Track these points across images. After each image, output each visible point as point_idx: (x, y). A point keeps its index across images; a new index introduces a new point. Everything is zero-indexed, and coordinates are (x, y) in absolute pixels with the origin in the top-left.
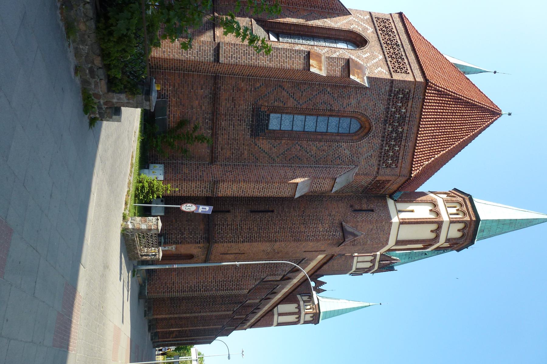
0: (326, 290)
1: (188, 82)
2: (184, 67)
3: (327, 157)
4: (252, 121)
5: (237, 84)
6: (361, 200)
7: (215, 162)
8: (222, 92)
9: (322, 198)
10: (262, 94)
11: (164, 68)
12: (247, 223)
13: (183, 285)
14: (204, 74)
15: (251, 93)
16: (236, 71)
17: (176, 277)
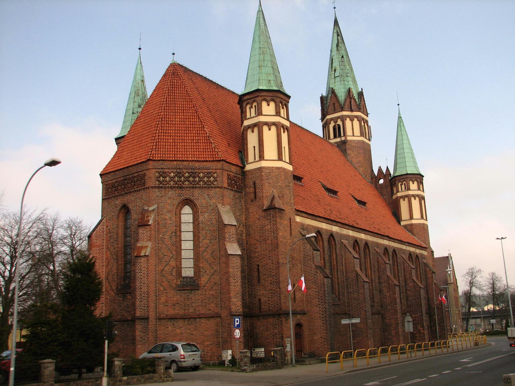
0: (387, 167)
2: (154, 341)
3: (211, 231)
4: (188, 290)
7: (219, 314)
8: (169, 313)
12: (267, 285)
13: (322, 330)
15: (168, 293)
16: (154, 305)
17: (317, 336)
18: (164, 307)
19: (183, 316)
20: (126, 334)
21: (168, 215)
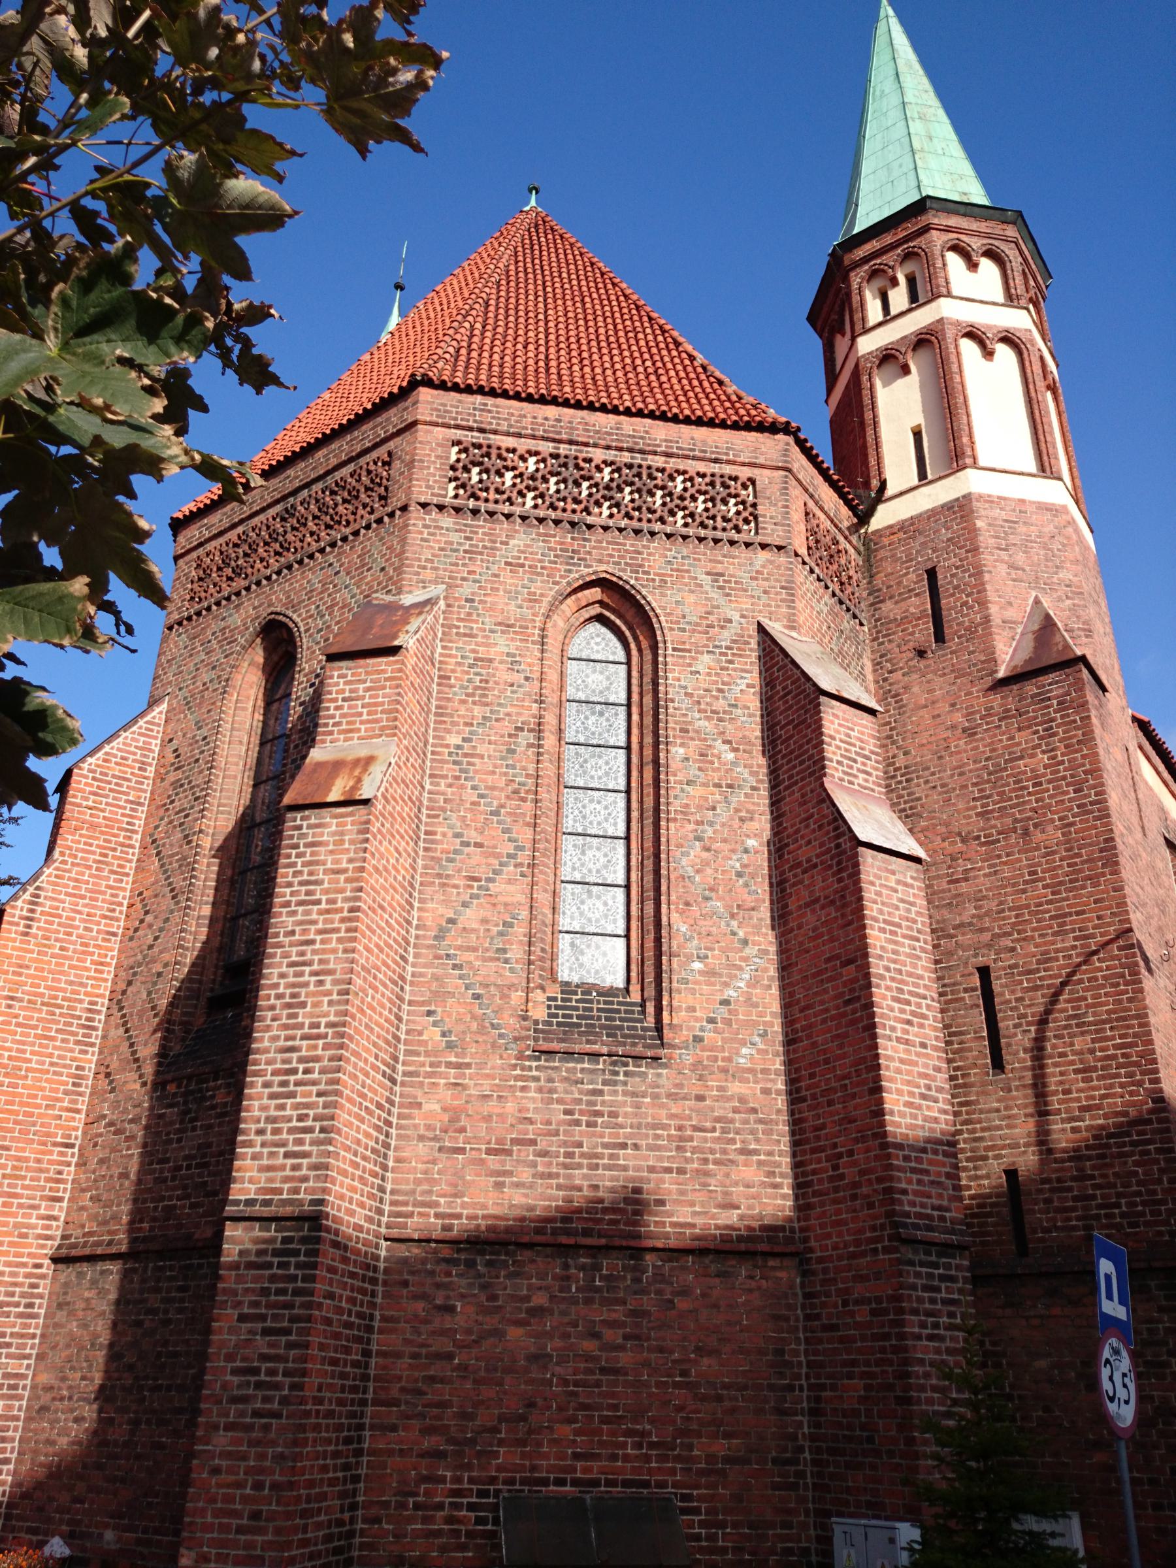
1: (416, 1381)
2: (341, 1402)
5: (430, 1134)
6: (890, 622)
8: (464, 1205)
9: (896, 770)
10: (474, 1017)
11: (347, 1515)
14: (379, 1300)
15: (468, 1066)
16: (368, 1135)
18: (434, 1162)
19: (555, 1232)
20: (166, 1343)
21: (502, 645)
